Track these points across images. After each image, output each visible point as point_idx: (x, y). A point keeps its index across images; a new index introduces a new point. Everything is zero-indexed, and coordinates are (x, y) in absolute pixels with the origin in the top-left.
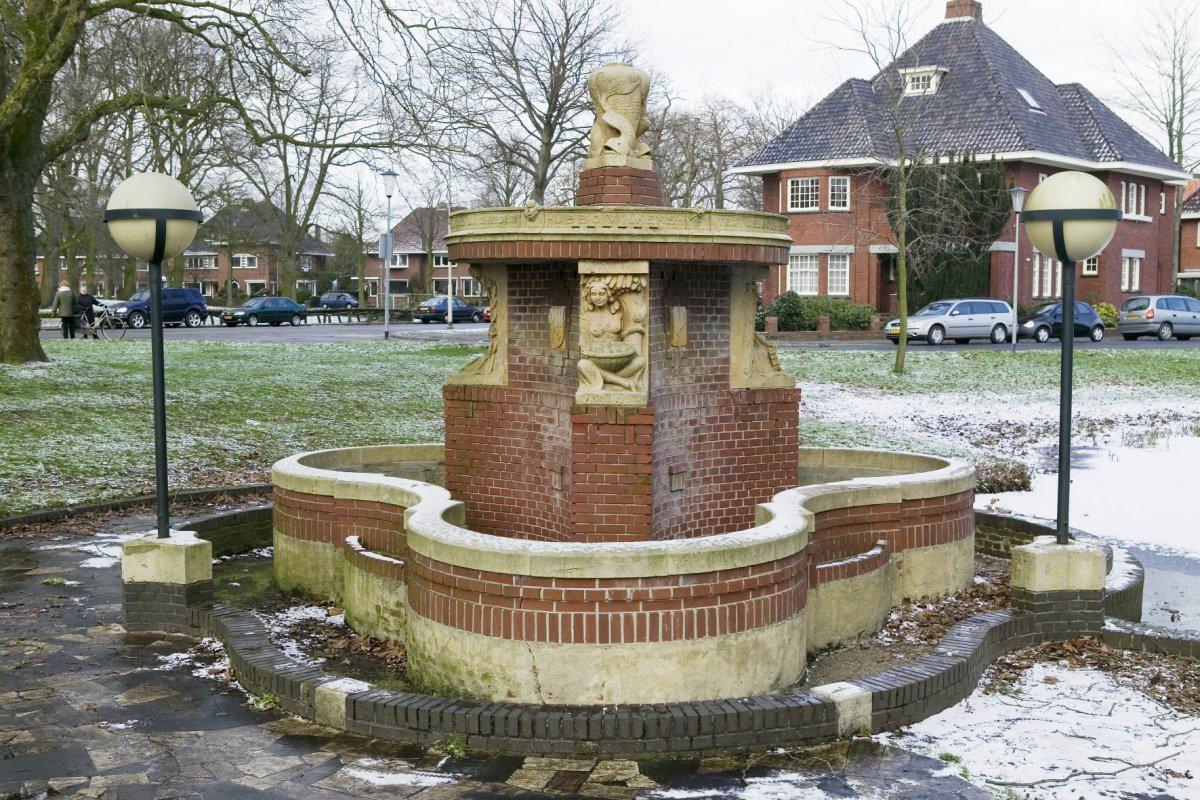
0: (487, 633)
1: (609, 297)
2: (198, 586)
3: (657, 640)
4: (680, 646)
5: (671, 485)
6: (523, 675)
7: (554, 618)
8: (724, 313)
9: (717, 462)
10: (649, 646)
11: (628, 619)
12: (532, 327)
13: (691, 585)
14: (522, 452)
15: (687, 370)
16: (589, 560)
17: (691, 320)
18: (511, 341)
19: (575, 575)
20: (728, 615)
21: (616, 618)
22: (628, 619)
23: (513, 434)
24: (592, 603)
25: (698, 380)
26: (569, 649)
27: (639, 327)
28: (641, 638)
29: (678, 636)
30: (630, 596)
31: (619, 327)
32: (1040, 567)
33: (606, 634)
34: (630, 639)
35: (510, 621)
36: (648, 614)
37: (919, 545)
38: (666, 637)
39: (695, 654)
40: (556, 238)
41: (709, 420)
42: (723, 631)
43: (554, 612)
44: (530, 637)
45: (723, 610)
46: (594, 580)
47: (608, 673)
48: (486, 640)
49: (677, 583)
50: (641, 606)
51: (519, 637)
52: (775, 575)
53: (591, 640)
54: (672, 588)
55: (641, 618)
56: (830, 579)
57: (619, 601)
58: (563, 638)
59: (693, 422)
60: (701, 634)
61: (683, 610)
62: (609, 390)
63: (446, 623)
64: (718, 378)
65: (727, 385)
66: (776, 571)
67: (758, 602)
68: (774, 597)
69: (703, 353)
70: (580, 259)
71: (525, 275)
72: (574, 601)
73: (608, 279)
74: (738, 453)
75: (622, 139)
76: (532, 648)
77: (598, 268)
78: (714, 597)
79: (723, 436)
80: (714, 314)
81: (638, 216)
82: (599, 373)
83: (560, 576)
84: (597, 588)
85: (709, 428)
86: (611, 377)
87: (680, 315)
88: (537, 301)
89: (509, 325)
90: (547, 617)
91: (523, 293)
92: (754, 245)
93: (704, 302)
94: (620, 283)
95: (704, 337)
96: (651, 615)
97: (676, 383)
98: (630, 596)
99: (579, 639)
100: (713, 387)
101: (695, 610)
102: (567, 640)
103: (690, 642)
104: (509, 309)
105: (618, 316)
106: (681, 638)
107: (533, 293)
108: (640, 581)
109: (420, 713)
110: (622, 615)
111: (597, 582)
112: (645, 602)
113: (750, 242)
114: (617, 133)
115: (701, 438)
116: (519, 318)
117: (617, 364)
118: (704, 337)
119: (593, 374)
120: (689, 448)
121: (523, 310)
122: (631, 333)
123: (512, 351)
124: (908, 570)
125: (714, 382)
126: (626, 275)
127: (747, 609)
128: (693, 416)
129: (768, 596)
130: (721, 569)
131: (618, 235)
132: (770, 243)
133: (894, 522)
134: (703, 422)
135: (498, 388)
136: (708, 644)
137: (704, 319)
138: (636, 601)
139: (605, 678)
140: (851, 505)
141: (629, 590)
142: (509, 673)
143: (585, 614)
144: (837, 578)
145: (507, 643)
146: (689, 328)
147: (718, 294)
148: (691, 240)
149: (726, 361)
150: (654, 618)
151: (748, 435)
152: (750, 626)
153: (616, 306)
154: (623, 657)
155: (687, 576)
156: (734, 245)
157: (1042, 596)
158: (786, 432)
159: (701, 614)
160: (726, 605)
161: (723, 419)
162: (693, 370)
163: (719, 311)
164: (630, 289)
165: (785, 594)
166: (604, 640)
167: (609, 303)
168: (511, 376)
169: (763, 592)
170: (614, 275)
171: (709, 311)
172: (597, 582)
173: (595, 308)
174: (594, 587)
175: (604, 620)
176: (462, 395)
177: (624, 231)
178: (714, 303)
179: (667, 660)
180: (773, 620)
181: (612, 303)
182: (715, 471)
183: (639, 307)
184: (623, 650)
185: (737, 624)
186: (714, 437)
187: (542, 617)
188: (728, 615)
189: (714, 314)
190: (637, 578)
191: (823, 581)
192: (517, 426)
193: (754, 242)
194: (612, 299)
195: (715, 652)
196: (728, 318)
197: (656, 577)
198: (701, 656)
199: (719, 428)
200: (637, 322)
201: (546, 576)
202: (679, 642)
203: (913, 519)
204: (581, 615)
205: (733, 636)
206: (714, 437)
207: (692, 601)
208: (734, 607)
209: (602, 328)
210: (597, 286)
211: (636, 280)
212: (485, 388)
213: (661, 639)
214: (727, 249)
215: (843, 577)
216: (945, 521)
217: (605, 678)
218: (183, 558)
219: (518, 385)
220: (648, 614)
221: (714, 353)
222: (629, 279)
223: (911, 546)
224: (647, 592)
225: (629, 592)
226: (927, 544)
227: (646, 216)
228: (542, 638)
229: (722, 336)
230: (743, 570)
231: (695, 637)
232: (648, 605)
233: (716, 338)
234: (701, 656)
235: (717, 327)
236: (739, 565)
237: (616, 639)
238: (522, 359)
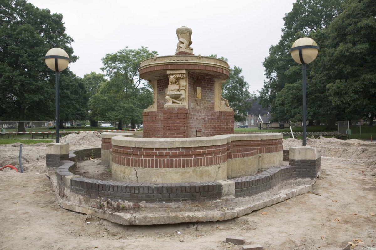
0: (124, 165)
1: (175, 80)
2: (64, 156)
3: (173, 167)
4: (181, 170)
5: (196, 134)
6: (133, 177)
7: (142, 160)
8: (213, 91)
9: (211, 130)
10: (170, 169)
11: (164, 161)
12: (162, 95)
13: (184, 151)
14: (160, 128)
15: (202, 105)
16: (152, 143)
17: (202, 91)
18: (158, 99)
19: (148, 147)
20: (196, 161)
21: (160, 160)
22: (164, 161)
23: (158, 123)
24: (153, 155)
25: (205, 108)
26: (147, 170)
27: (184, 88)
28: (168, 167)
29: (180, 166)
30: (164, 154)
31: (178, 88)
32: (297, 153)
33: (157, 165)
34: (164, 167)
35: (130, 161)
36: (170, 159)
37: (266, 152)
38: (176, 167)
39: (186, 172)
40: (161, 64)
41: (208, 118)
42: (195, 166)
43: (142, 158)
44: (135, 166)
45: (194, 160)
46: (153, 148)
47: (158, 177)
48: (124, 167)
49: (179, 150)
50: (168, 157)
51: (132, 166)
52: (213, 150)
53: (153, 167)
54: (177, 152)
55: (168, 160)
56: (236, 157)
57: (161, 155)
58: (138, 166)
59: (203, 119)
60: (187, 166)
61: (181, 159)
62: (174, 104)
63: (116, 163)
64: (211, 108)
65: (214, 110)
66: (213, 149)
67: (207, 158)
68: (213, 157)
69: (207, 101)
70: (167, 70)
71: (161, 82)
72: (148, 155)
73: (175, 75)
74: (217, 128)
75: (184, 45)
76: (136, 169)
77: (172, 72)
78: (192, 155)
79: (212, 123)
80: (210, 91)
81: (182, 57)
82: (171, 100)
83: (144, 147)
84: (155, 151)
85: (208, 121)
86: (175, 101)
87: (199, 90)
88: (163, 88)
89: (157, 95)
90: (140, 160)
91: (160, 86)
92: (216, 67)
93: (207, 87)
94: (178, 76)
95: (207, 96)
96: (171, 160)
97: (198, 107)
98: (164, 154)
99: (149, 167)
100: (209, 110)
101: (185, 159)
102: (146, 167)
103: (183, 168)
104: (157, 91)
105: (178, 86)
106: (181, 167)
107: (163, 86)
108: (168, 149)
109: (87, 184)
110: (162, 159)
111: (155, 149)
112: (169, 156)
113: (215, 66)
114: (183, 43)
115: (206, 123)
116: (159, 93)
117: (176, 97)
118: (207, 96)
119: (170, 100)
120: (202, 125)
121: (160, 91)
122: (181, 90)
123: (158, 102)
124: (263, 159)
125: (210, 109)
126: (179, 74)
127: (203, 160)
128: (203, 117)
129: (210, 157)
130: (194, 146)
131: (177, 62)
132: (221, 67)
133: (258, 145)
134: (207, 119)
135: (154, 112)
136: (190, 169)
137: (207, 92)
138: (166, 155)
139: (157, 179)
140: (246, 140)
141: (164, 152)
142: (130, 177)
143: (151, 159)
144: (238, 157)
145: (129, 168)
146: (202, 94)
147: (211, 86)
148: (197, 64)
149: (213, 103)
150: (172, 161)
151: (219, 123)
152: (204, 165)
153: (178, 83)
154: (162, 173)
155: (183, 148)
156: (210, 66)
157: (298, 161)
158: (230, 123)
159: (187, 160)
160: (196, 158)
161: (212, 119)
162: (203, 105)
163: (211, 90)
164: (181, 78)
165: (217, 157)
166: (156, 167)
167: (176, 82)
168: (158, 108)
169: (209, 155)
170: (177, 74)
171: (208, 90)
172: (155, 149)
173: (172, 83)
174: (158, 152)
175: (156, 160)
176: (147, 114)
177: (179, 61)
178: (210, 88)
179: (176, 174)
180: (212, 164)
181: (177, 82)
182: (210, 133)
183: (184, 83)
184: (163, 170)
185: (200, 164)
186: (210, 123)
187: (139, 160)
188: (196, 161)
189: (210, 91)
190: (167, 148)
191: (234, 157)
192: (159, 121)
193: (217, 66)
194: (176, 81)
195: (192, 172)
196: (214, 92)
197: (172, 148)
198: (187, 173)
199: (211, 121)
200: (183, 87)
201: (140, 147)
202: (180, 168)
203: (264, 145)
204: (150, 159)
205: (198, 168)
206: (210, 123)
207: (184, 156)
208: (198, 159)
209: (174, 88)
210: (172, 77)
211: (182, 75)
212: (152, 112)
213: (174, 167)
214: (209, 67)
215: (240, 157)
216: (273, 146)
217: (157, 179)
218: (59, 147)
219: (159, 110)
220: (170, 159)
221: (210, 101)
222: (180, 75)
223: (264, 152)
224: (170, 152)
225: (164, 152)
226: (268, 152)
227: (185, 57)
228: (139, 166)
229: (212, 97)
230: (202, 148)
231: (185, 167)
232: (170, 156)
233: (210, 97)
234: (187, 173)
235: (211, 94)
236: (200, 146)
237: (160, 167)
238: (160, 104)
